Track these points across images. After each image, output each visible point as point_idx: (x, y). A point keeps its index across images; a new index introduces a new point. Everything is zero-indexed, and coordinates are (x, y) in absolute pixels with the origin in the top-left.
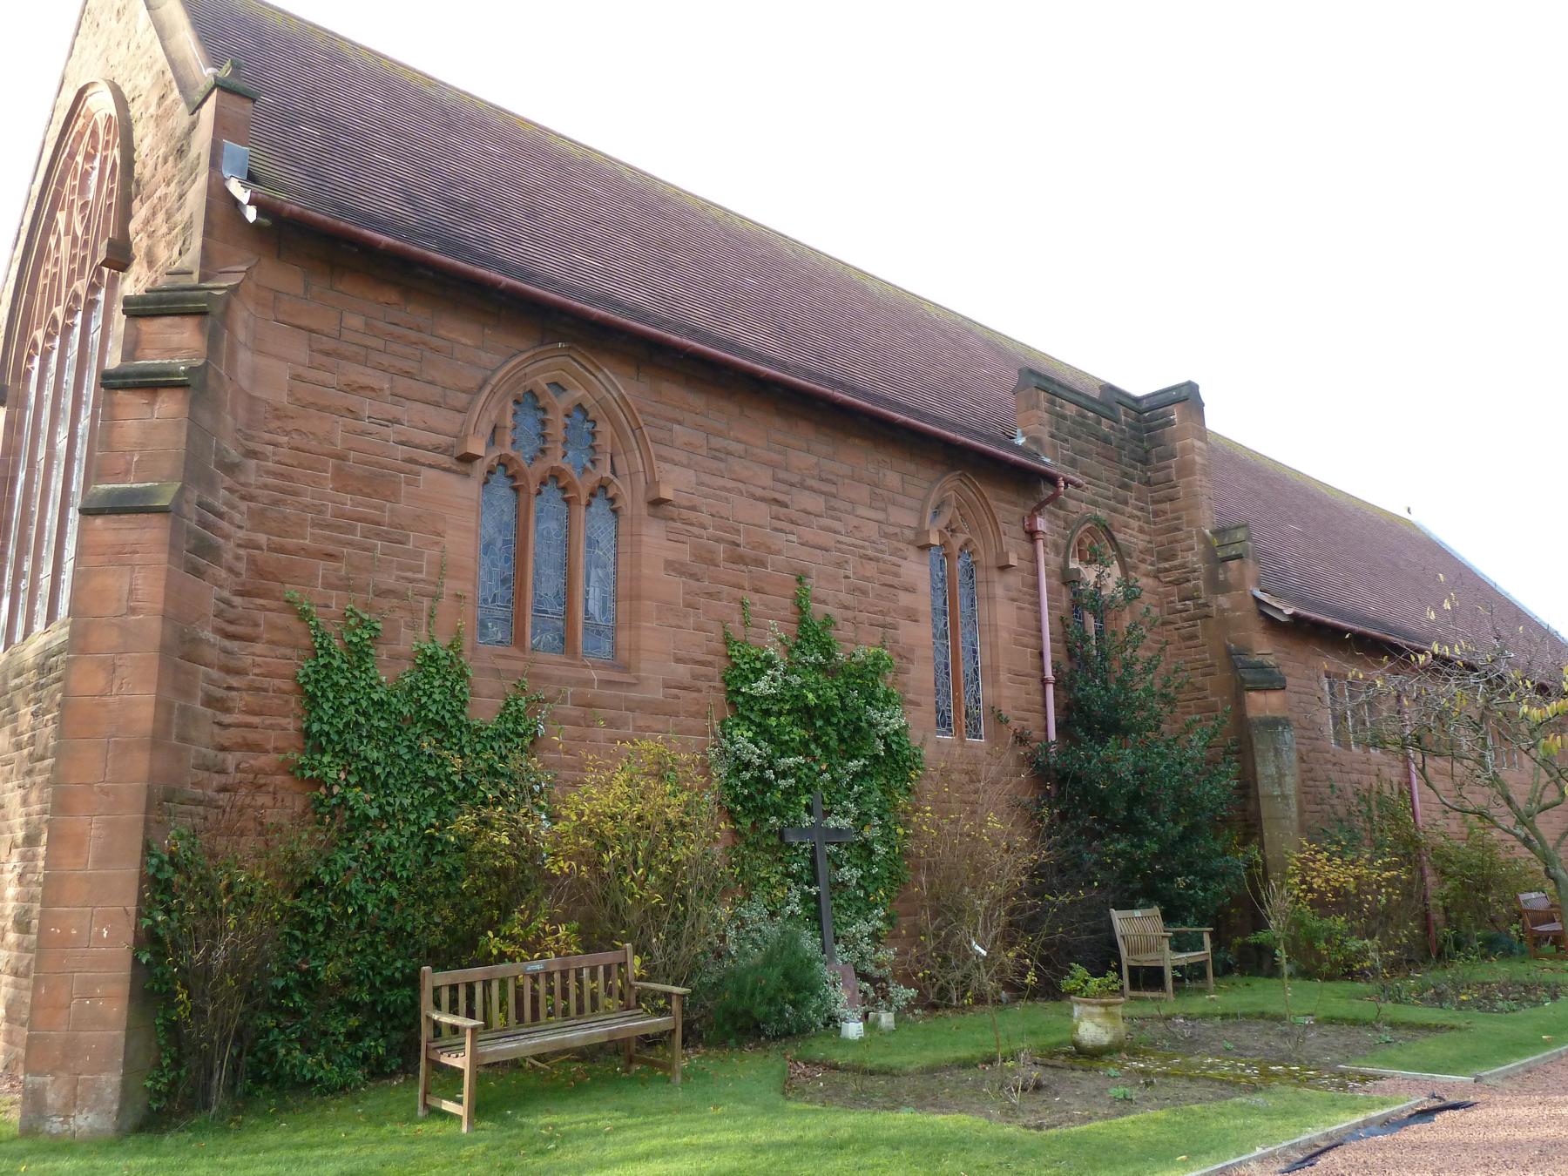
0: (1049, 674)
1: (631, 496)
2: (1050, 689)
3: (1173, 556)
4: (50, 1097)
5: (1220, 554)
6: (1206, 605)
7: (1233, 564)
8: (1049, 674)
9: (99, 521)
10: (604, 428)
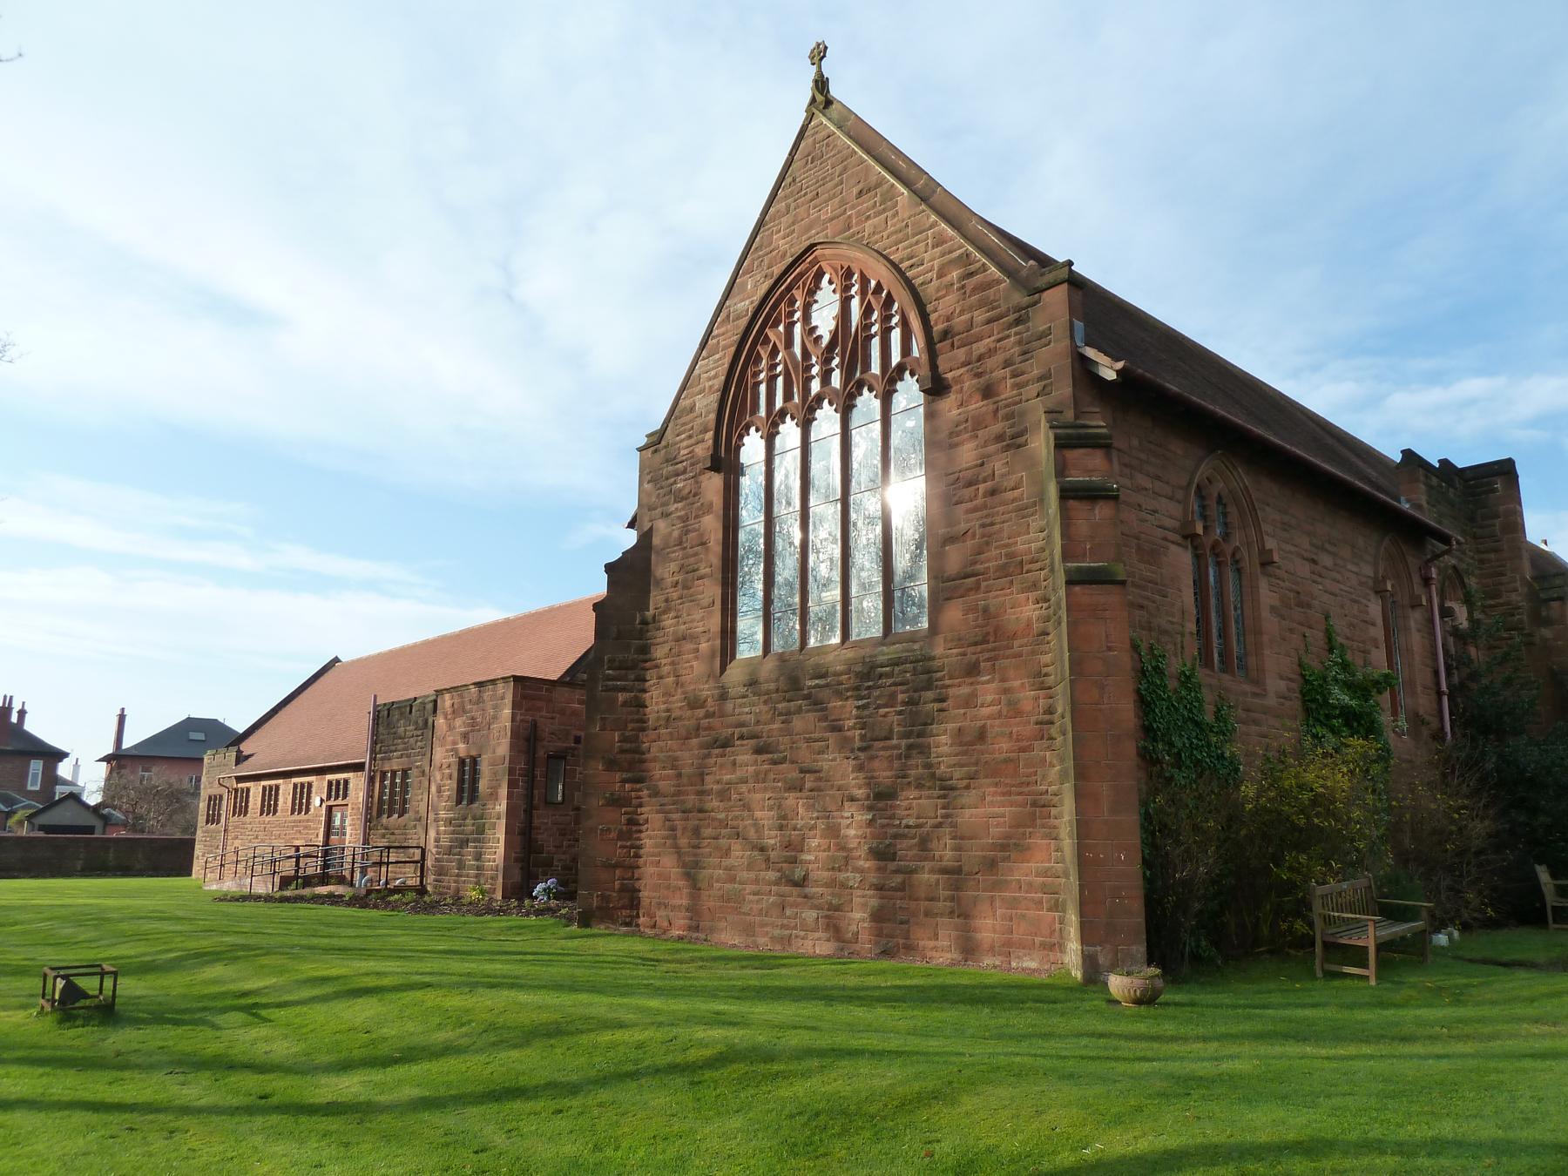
0: (1444, 688)
1: (1250, 561)
2: (1445, 699)
3: (1497, 595)
4: (1101, 960)
5: (1542, 596)
6: (1530, 635)
7: (1555, 604)
8: (1444, 688)
9: (1077, 589)
10: (1232, 509)
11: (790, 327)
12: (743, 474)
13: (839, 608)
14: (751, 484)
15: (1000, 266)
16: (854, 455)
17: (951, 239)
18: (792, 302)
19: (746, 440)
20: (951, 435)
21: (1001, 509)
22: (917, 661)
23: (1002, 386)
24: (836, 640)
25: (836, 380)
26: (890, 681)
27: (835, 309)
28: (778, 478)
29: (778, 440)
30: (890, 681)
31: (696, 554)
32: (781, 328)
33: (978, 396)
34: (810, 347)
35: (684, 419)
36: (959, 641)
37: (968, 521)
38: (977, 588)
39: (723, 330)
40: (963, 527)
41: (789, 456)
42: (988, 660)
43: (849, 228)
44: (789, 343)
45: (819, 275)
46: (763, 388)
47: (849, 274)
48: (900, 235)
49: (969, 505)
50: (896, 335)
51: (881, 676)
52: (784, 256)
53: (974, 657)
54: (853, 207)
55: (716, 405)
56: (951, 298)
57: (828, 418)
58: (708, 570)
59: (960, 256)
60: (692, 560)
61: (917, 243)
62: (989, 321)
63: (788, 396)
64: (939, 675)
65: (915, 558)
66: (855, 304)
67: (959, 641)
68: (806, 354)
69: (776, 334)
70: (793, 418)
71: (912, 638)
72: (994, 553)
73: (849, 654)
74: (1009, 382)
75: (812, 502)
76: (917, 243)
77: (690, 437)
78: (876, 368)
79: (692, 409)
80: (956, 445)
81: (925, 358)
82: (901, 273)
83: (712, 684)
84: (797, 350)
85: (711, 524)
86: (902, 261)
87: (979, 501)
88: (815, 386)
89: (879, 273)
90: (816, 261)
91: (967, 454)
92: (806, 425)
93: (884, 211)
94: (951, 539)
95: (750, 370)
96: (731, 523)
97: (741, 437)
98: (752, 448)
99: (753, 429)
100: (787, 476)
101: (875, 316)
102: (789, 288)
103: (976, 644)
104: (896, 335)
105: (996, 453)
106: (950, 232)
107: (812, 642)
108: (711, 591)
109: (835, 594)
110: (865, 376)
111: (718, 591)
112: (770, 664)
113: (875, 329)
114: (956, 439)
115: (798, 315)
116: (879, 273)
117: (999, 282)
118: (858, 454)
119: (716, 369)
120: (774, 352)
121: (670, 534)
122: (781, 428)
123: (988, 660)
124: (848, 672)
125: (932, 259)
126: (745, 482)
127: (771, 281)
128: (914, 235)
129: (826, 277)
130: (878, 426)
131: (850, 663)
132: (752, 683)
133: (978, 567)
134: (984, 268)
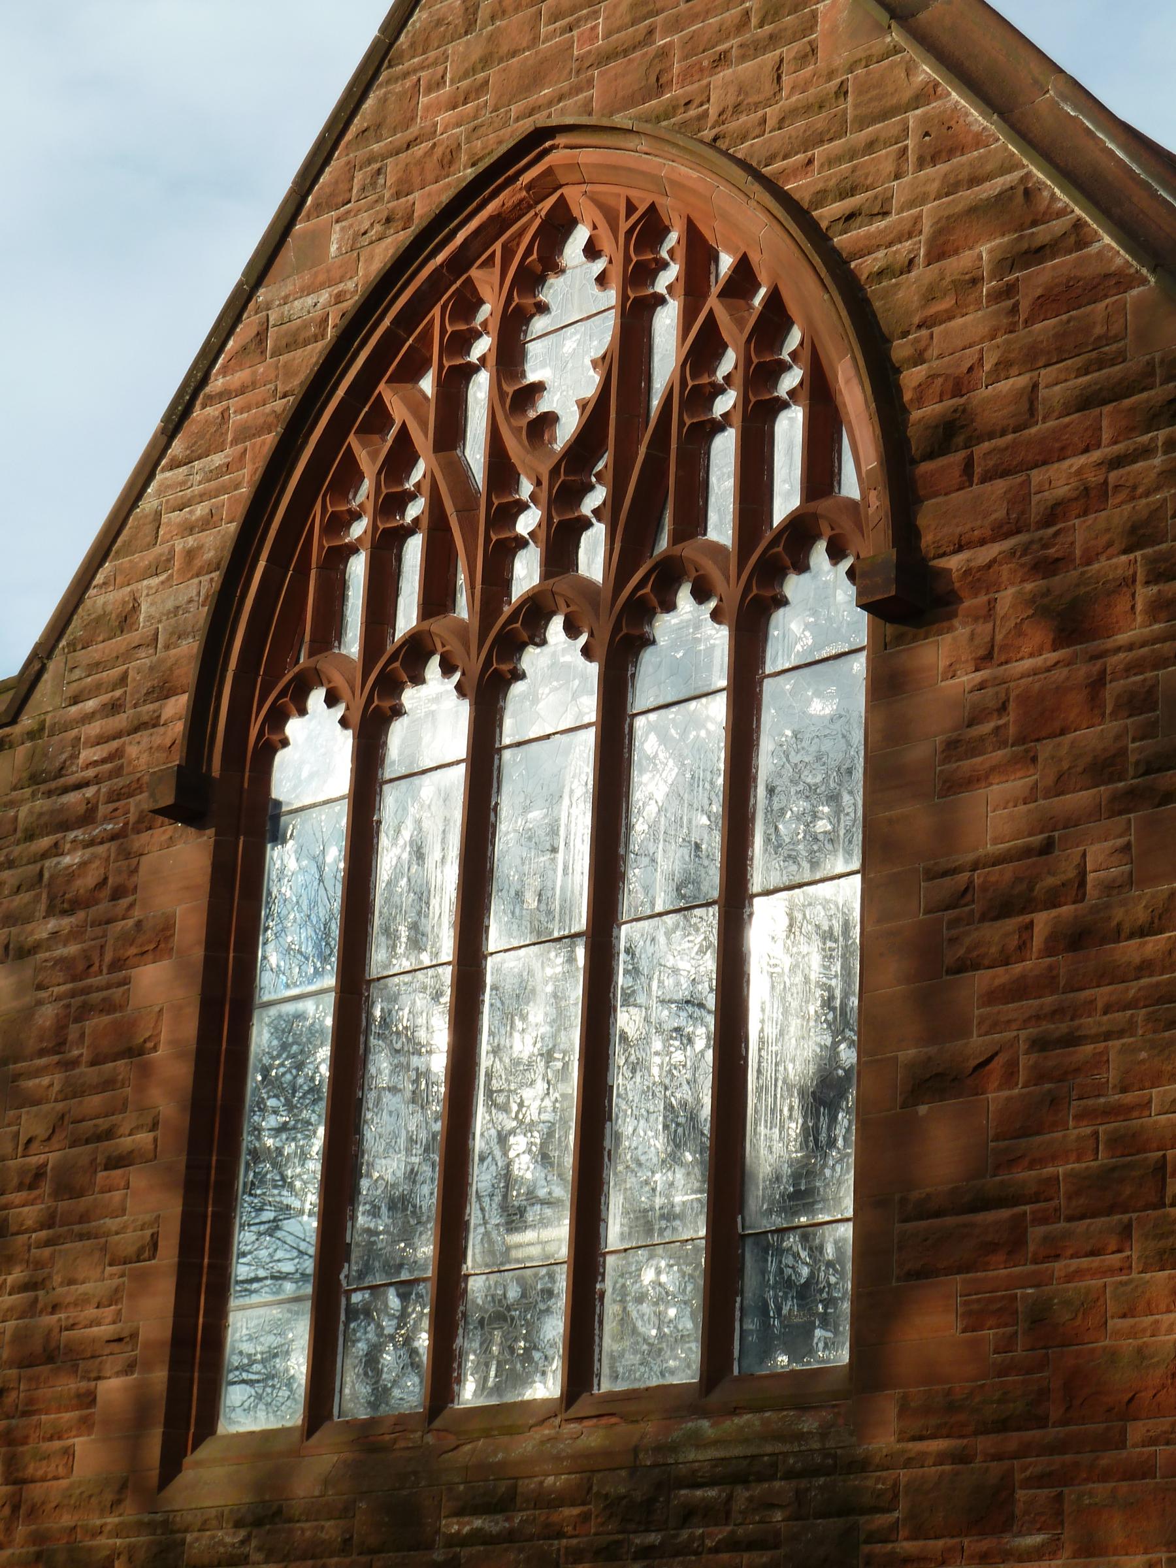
11: (455, 384)
12: (278, 837)
13: (562, 1283)
14: (301, 873)
15: (1129, 231)
16: (638, 795)
17: (979, 141)
18: (468, 303)
19: (294, 727)
20: (954, 748)
21: (1103, 993)
22: (814, 1472)
23: (1121, 605)
24: (546, 1387)
25: (593, 557)
26: (721, 1533)
27: (601, 336)
28: (389, 857)
29: (397, 735)
30: (721, 1533)
31: (109, 1084)
32: (427, 384)
33: (1038, 635)
34: (514, 447)
35: (97, 652)
36: (944, 1412)
37: (995, 1026)
38: (1013, 1243)
39: (240, 377)
40: (977, 1043)
41: (428, 787)
42: (1040, 1480)
43: (660, 87)
44: (450, 432)
45: (559, 226)
46: (358, 568)
47: (650, 228)
48: (819, 121)
49: (1001, 976)
50: (790, 428)
51: (689, 1514)
52: (448, 161)
53: (996, 1469)
54: (676, 25)
55: (200, 615)
56: (972, 322)
57: (558, 670)
58: (144, 1138)
59: (1003, 199)
60: (95, 1101)
61: (871, 146)
62: (1086, 402)
63: (436, 598)
64: (882, 1520)
65: (816, 1141)
66: (666, 324)
67: (944, 1412)
68: (501, 469)
69: (410, 402)
70: (447, 669)
71: (802, 1391)
72: (1077, 1131)
73: (591, 1437)
74: (1144, 594)
75: (496, 936)
76: (871, 146)
77: (114, 708)
78: (721, 527)
79: (126, 619)
80: (971, 782)
81: (877, 503)
82: (816, 236)
83: (129, 1513)
84: (475, 453)
85: (161, 991)
86: (821, 198)
87: (1030, 966)
88: (526, 572)
89: (747, 232)
90: (548, 184)
91: (996, 815)
92: (487, 697)
93: (773, 40)
94: (936, 1082)
95: (327, 494)
96: (228, 989)
97: (278, 719)
98: (313, 756)
99: (316, 698)
100: (419, 854)
101: (728, 363)
102: (460, 263)
103: (1003, 1425)
104: (790, 428)
105: (1096, 813)
106: (977, 118)
107: (469, 1393)
108: (143, 1205)
109: (553, 1236)
110: (687, 550)
111: (172, 1208)
112: (326, 1457)
113: (725, 403)
114: (968, 765)
115: (483, 346)
116: (747, 232)
117: (1122, 281)
118: (650, 788)
119: (211, 497)
120: (402, 457)
121: (28, 1014)
122: (410, 697)
123: (1040, 1480)
124: (579, 1495)
125: (913, 200)
126: (283, 860)
127: (404, 237)
128: (863, 122)
129: (580, 236)
130: (717, 710)
131: (588, 1466)
132: (265, 1515)
133: (1024, 1176)
134: (1078, 236)
